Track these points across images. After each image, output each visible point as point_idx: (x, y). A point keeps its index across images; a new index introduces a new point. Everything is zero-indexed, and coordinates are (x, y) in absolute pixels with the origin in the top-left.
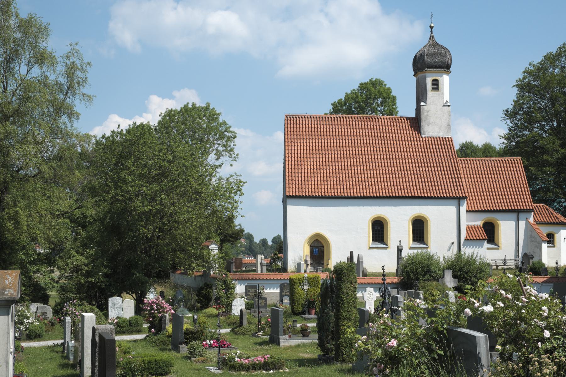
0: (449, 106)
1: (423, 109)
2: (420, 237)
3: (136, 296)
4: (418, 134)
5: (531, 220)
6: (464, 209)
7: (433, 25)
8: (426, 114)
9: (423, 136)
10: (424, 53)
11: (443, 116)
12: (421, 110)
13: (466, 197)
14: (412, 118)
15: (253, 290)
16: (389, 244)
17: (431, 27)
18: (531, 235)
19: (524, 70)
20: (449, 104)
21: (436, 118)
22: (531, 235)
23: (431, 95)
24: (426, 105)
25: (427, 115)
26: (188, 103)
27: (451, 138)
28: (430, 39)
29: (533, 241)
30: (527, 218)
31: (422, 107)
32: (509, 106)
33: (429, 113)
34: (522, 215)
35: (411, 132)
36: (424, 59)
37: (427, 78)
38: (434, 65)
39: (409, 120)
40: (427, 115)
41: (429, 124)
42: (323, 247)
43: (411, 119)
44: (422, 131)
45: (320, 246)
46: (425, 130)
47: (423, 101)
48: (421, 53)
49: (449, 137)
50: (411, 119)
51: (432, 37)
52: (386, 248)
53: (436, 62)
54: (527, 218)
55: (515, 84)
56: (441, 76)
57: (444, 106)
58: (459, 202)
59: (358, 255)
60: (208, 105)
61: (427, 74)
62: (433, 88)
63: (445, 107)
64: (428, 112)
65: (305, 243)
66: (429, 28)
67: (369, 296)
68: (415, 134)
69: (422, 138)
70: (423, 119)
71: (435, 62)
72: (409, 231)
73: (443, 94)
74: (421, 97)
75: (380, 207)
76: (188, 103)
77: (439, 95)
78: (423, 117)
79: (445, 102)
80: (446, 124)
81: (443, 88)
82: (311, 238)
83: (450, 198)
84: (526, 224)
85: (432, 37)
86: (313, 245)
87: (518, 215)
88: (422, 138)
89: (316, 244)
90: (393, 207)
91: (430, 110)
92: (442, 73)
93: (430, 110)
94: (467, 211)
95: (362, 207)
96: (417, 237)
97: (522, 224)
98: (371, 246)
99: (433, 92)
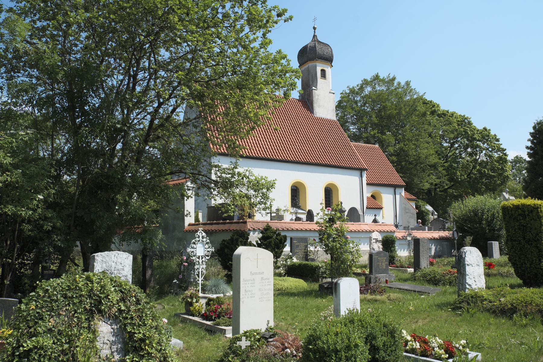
0: (334, 93)
3: (466, 285)
7: (316, 26)
8: (317, 97)
13: (366, 170)
15: (302, 245)
17: (315, 28)
18: (405, 208)
22: (405, 208)
25: (318, 99)
29: (407, 213)
31: (314, 91)
32: (413, 85)
34: (398, 190)
36: (316, 50)
37: (318, 68)
38: (322, 57)
41: (319, 106)
44: (314, 112)
46: (317, 111)
51: (315, 36)
53: (324, 55)
61: (318, 64)
62: (322, 76)
64: (318, 96)
71: (324, 54)
73: (329, 82)
85: (315, 36)
97: (398, 197)
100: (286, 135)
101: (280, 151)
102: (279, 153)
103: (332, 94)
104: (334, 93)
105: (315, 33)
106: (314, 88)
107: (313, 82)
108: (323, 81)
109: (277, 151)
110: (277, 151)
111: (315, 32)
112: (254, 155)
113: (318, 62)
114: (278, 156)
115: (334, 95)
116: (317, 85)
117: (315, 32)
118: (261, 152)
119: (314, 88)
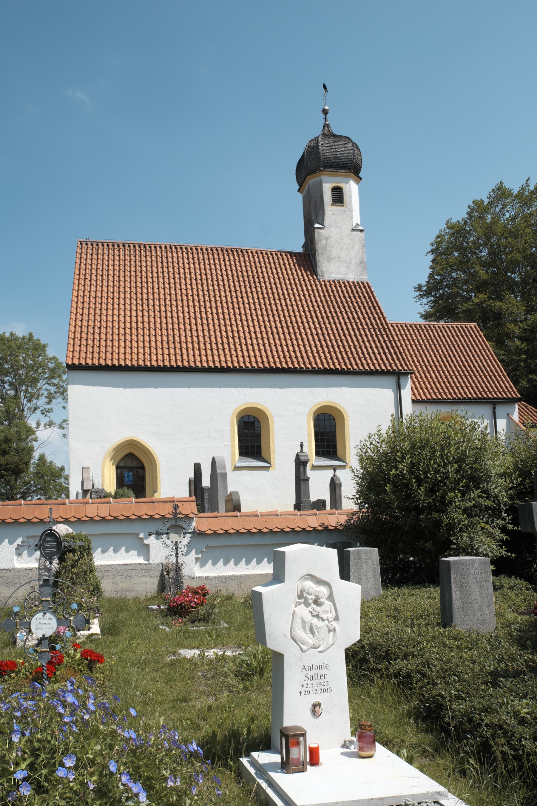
0: (361, 231)
1: (319, 233)
2: (329, 447)
4: (312, 276)
5: (516, 416)
6: (407, 394)
8: (324, 242)
9: (321, 279)
10: (317, 143)
11: (353, 247)
12: (316, 236)
13: (411, 372)
14: (300, 254)
16: (272, 460)
17: (325, 112)
19: (438, 233)
20: (361, 228)
21: (342, 250)
23: (331, 212)
24: (323, 228)
26: (4, 333)
27: (367, 283)
28: (324, 128)
30: (508, 414)
31: (316, 231)
32: (423, 280)
33: (329, 242)
34: (500, 409)
35: (300, 273)
36: (318, 152)
39: (295, 256)
40: (326, 244)
41: (329, 260)
42: (143, 468)
43: (298, 255)
45: (136, 468)
46: (324, 269)
47: (318, 223)
48: (312, 144)
49: (364, 281)
50: (298, 255)
51: (326, 126)
52: (267, 468)
53: (338, 158)
54: (508, 414)
55: (429, 249)
56: (347, 183)
57: (353, 230)
58: (399, 380)
59: (214, 460)
60: (31, 334)
61: (324, 178)
62: (334, 201)
63: (355, 233)
64: (327, 239)
65: (105, 459)
66: (322, 113)
67: (303, 611)
68: (307, 276)
69: (319, 281)
70: (320, 252)
71: (336, 158)
72: (309, 435)
73: (351, 210)
74: (313, 217)
75: (253, 389)
76: (4, 333)
77: (345, 212)
78: (320, 244)
79: (354, 224)
80: (358, 260)
81: (351, 201)
82: (118, 449)
83: (382, 373)
84: (508, 425)
86: (122, 464)
87: (494, 409)
88: (319, 281)
89: (129, 464)
90: (277, 390)
91: (330, 237)
92: (349, 176)
93: (330, 237)
94: (413, 402)
95: (217, 389)
96: (323, 446)
98: (238, 465)
99: (335, 207)
100: (448, 336)
101: (475, 379)
102: (474, 382)
103: (359, 233)
104: (361, 231)
105: (326, 121)
106: (317, 225)
107: (316, 216)
108: (338, 209)
109: (480, 379)
110: (470, 380)
111: (325, 118)
112: (439, 396)
113: (325, 175)
114: (495, 393)
115: (363, 233)
116: (324, 219)
117: (325, 118)
118: (456, 390)
119: (317, 225)
